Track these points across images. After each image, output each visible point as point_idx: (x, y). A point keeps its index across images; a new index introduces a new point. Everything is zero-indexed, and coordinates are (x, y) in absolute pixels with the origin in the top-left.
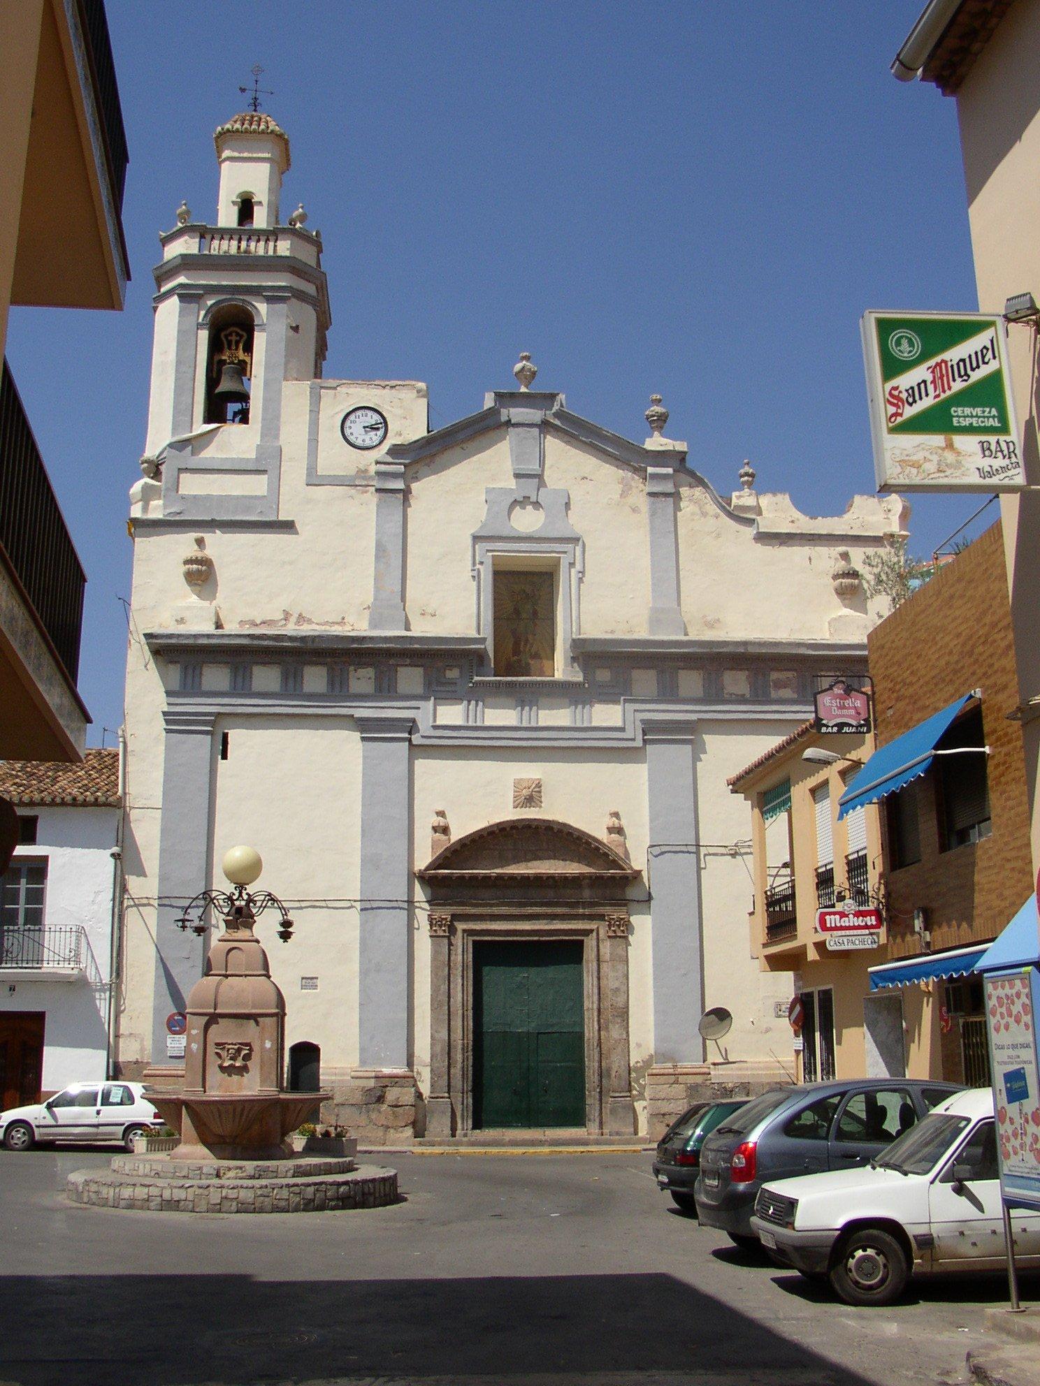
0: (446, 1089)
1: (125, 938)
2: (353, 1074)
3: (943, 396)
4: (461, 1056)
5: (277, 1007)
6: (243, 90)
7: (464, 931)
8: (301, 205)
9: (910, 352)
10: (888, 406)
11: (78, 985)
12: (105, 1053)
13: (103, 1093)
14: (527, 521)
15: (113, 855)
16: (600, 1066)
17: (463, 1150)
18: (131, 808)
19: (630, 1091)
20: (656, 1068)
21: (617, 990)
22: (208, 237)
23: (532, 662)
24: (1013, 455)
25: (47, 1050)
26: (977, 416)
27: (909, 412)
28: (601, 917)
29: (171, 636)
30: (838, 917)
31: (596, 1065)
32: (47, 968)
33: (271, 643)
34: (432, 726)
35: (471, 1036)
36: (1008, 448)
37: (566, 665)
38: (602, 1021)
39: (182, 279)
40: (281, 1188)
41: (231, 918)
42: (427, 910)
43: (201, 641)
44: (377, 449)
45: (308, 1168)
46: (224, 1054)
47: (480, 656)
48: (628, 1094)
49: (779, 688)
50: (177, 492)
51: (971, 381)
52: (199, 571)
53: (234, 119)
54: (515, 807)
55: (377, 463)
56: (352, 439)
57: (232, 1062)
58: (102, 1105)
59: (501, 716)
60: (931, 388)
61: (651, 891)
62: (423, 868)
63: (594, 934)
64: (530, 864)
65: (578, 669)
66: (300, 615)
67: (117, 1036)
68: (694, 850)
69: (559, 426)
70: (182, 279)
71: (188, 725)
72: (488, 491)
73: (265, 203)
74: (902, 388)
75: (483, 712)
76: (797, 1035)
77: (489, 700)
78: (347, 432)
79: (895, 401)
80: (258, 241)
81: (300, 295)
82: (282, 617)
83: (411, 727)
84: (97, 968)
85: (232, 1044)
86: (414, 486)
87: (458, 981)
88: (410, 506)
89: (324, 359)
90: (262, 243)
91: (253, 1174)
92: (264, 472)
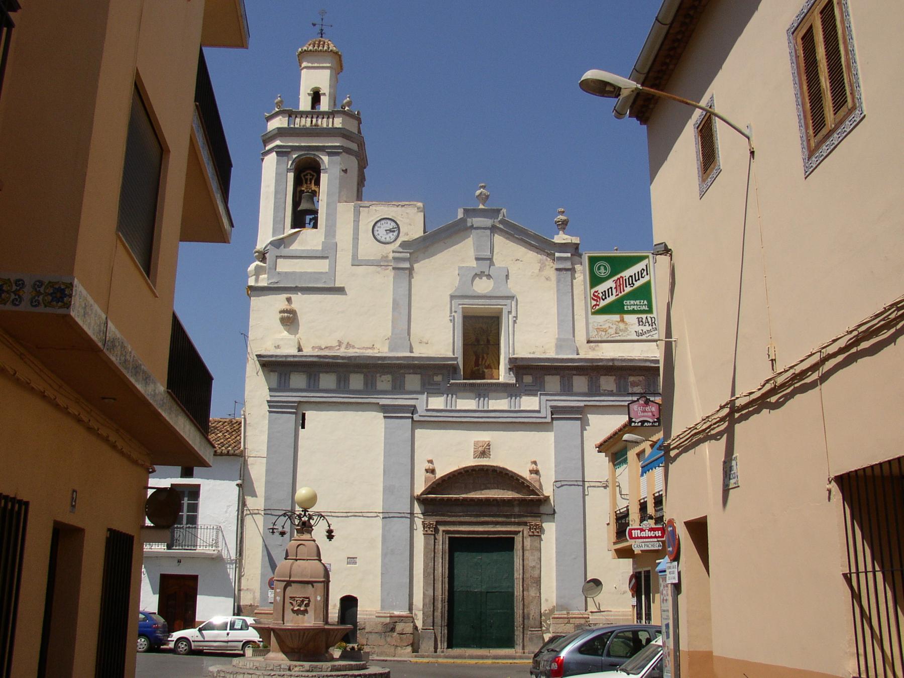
0: (432, 624)
1: (244, 533)
2: (377, 615)
3: (620, 295)
4: (441, 605)
5: (324, 578)
6: (314, 25)
7: (443, 531)
8: (348, 96)
9: (605, 273)
10: (592, 301)
11: (217, 560)
12: (233, 600)
13: (231, 623)
14: (483, 286)
15: (237, 485)
16: (523, 612)
17: (440, 660)
18: (248, 457)
19: (541, 627)
20: (557, 614)
21: (534, 567)
22: (294, 116)
23: (486, 371)
24: (654, 324)
25: (199, 598)
26: (637, 305)
27: (602, 304)
28: (525, 524)
29: (272, 356)
30: (639, 531)
31: (521, 612)
32: (199, 550)
33: (330, 360)
34: (426, 410)
35: (447, 593)
36: (652, 321)
37: (505, 373)
38: (525, 585)
39: (278, 142)
40: (324, 677)
41: (299, 527)
42: (421, 518)
43: (289, 359)
44: (393, 244)
45: (339, 667)
46: (294, 603)
47: (452, 370)
48: (540, 629)
49: (634, 386)
50: (276, 269)
51: (634, 287)
52: (288, 318)
53: (309, 43)
54: (474, 458)
55: (394, 252)
56: (379, 237)
57: (298, 608)
58: (230, 629)
59: (467, 404)
60: (614, 291)
61: (555, 508)
62: (419, 494)
63: (521, 533)
64: (483, 492)
65: (512, 375)
66: (348, 343)
67: (240, 590)
68: (581, 484)
69: (502, 229)
70: (278, 142)
71: (282, 409)
72: (460, 268)
73: (327, 94)
74: (600, 292)
75: (456, 402)
76: (633, 596)
77: (459, 394)
78: (376, 233)
79: (596, 298)
80: (323, 118)
81: (348, 151)
82: (337, 344)
83: (413, 410)
84: (228, 550)
85: (299, 598)
86: (416, 266)
87: (439, 560)
88: (413, 278)
89: (364, 186)
90: (325, 120)
91: (308, 669)
92: (327, 258)
